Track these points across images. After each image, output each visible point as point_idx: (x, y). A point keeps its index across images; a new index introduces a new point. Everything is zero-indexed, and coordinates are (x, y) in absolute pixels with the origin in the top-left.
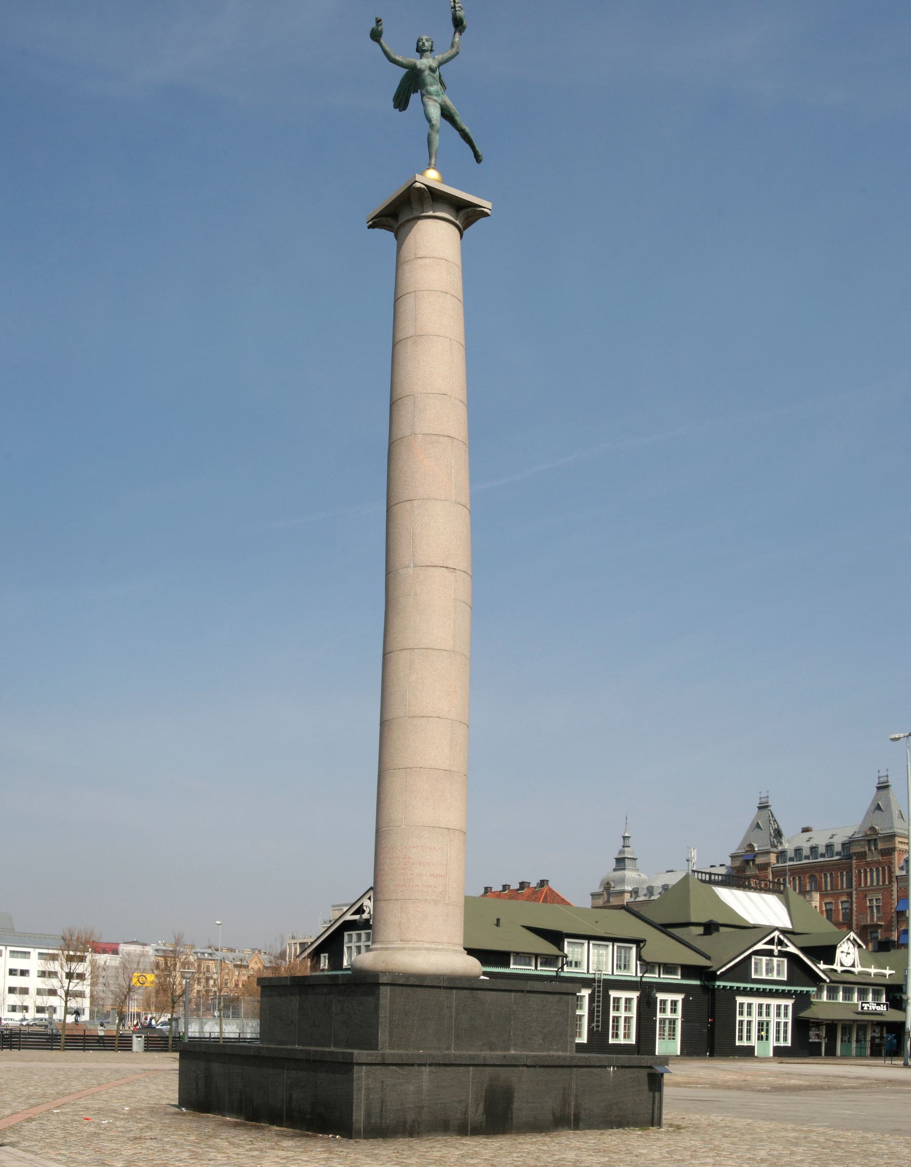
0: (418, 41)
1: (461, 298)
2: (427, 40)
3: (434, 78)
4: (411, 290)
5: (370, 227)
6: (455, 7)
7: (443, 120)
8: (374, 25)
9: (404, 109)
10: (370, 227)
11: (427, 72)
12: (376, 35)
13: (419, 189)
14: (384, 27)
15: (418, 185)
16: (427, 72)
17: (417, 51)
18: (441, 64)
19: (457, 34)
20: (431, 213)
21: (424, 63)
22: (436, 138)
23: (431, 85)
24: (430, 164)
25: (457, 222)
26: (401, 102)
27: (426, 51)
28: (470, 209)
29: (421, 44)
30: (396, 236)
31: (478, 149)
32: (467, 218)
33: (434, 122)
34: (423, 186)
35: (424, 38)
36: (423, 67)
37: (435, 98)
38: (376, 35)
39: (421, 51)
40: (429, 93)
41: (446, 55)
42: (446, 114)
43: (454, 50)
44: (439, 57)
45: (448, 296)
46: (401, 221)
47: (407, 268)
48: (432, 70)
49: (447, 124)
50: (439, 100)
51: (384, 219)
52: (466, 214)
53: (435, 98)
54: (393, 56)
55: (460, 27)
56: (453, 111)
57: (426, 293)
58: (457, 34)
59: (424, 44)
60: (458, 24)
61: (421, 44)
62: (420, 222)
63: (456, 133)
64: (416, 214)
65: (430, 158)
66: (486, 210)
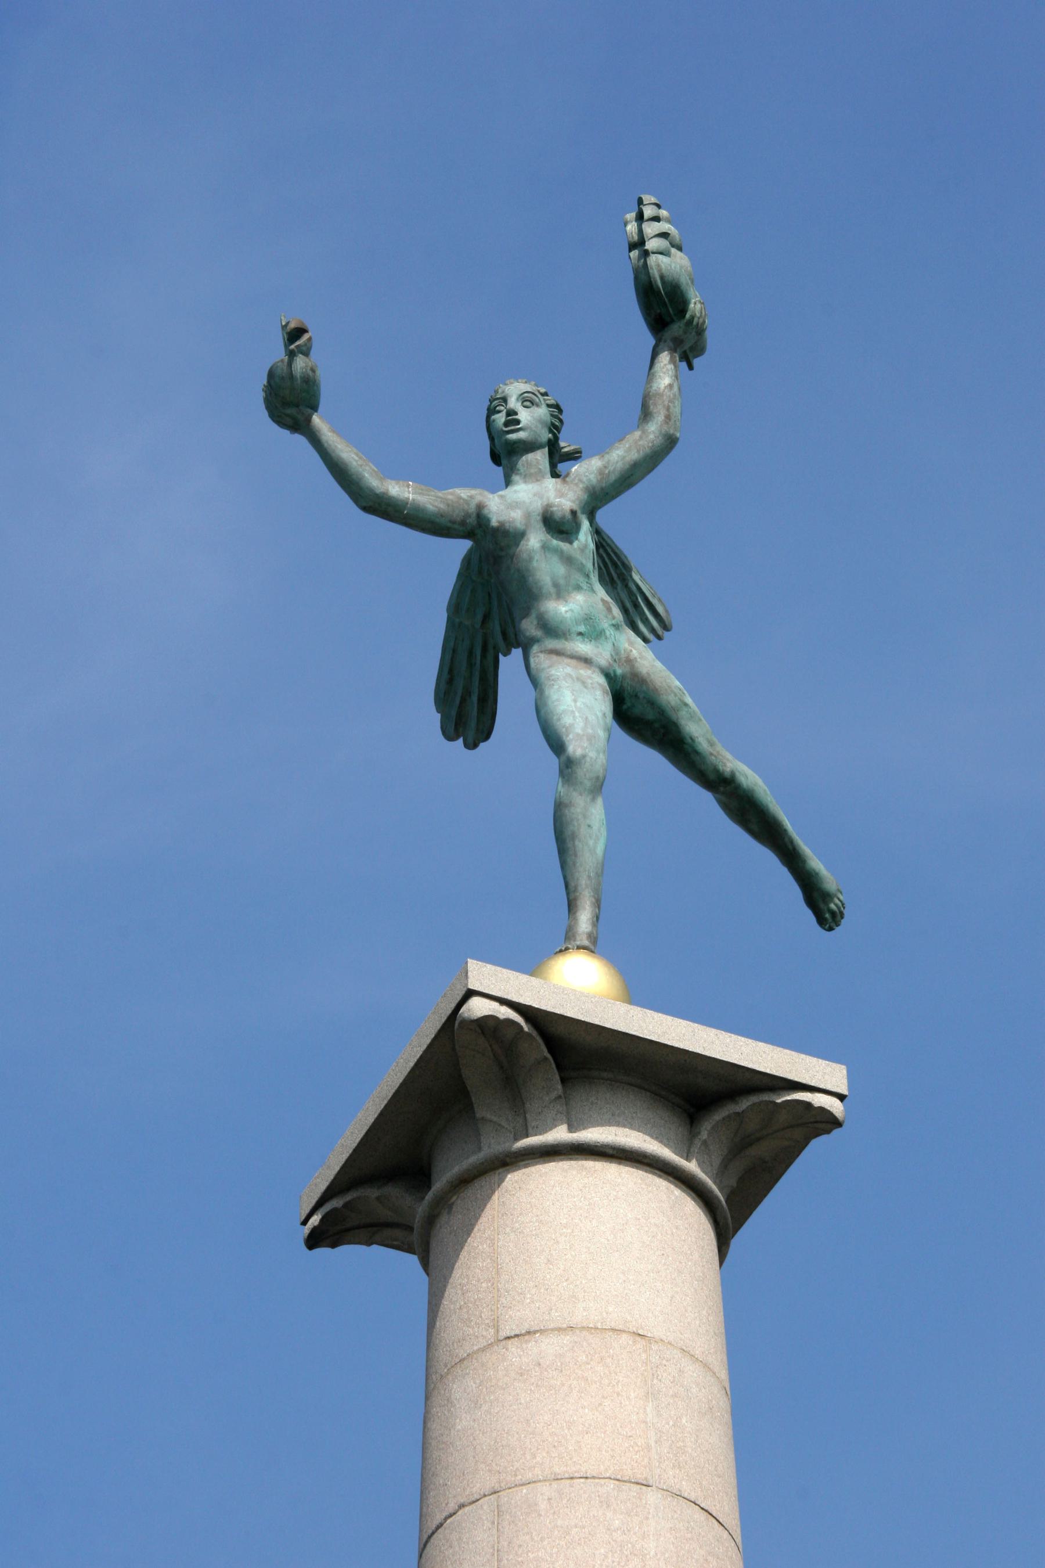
0: (492, 411)
1: (727, 1506)
2: (528, 401)
3: (568, 560)
4: (476, 1489)
5: (314, 1241)
6: (639, 244)
7: (620, 733)
8: (278, 353)
9: (485, 732)
10: (314, 1241)
11: (535, 540)
12: (291, 402)
13: (487, 1025)
14: (325, 362)
15: (478, 1008)
16: (535, 540)
17: (496, 458)
18: (598, 498)
19: (664, 358)
20: (560, 1134)
21: (521, 499)
22: (592, 821)
23: (560, 593)
24: (570, 934)
25: (692, 1167)
26: (467, 705)
27: (529, 447)
28: (745, 1104)
29: (500, 419)
30: (425, 1264)
31: (815, 863)
32: (739, 1146)
33: (574, 748)
34: (505, 1013)
35: (514, 390)
36: (515, 517)
37: (583, 647)
38: (291, 402)
39: (505, 454)
40: (551, 629)
41: (621, 455)
42: (636, 712)
43: (653, 430)
44: (587, 470)
45: (652, 1497)
46: (439, 1185)
47: (460, 1389)
48: (559, 527)
49: (653, 761)
50: (601, 653)
51: (371, 1193)
52: (735, 1139)
53: (583, 647)
54: (373, 480)
55: (676, 329)
56: (669, 700)
57: (546, 1490)
58: (664, 358)
59: (512, 420)
60: (664, 310)
61: (500, 419)
62: (513, 1179)
63: (706, 800)
64: (492, 1146)
65: (572, 906)
66: (819, 1100)
